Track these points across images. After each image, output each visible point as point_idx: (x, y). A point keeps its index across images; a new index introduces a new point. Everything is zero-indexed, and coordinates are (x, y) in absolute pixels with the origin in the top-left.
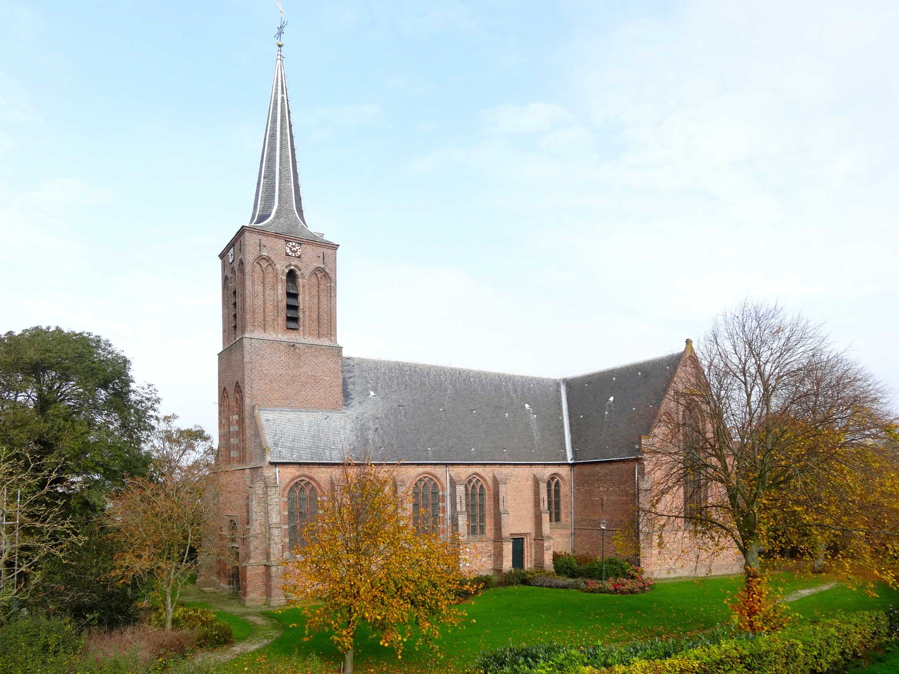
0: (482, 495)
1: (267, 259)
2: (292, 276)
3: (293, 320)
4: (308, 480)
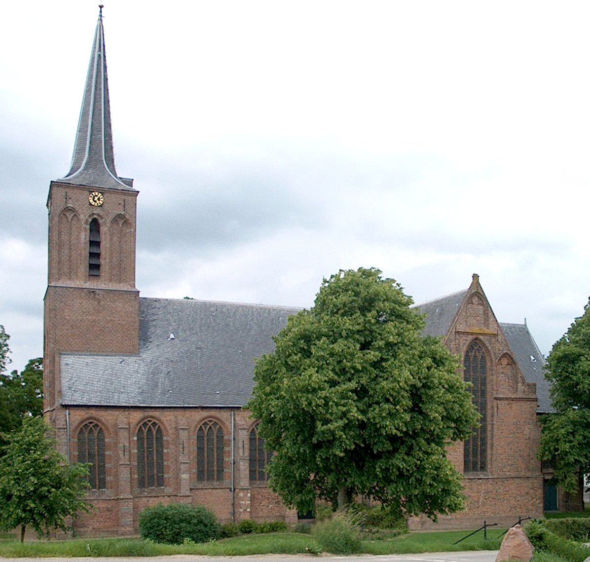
1: (72, 210)
2: (95, 226)
3: (94, 268)
4: (96, 422)
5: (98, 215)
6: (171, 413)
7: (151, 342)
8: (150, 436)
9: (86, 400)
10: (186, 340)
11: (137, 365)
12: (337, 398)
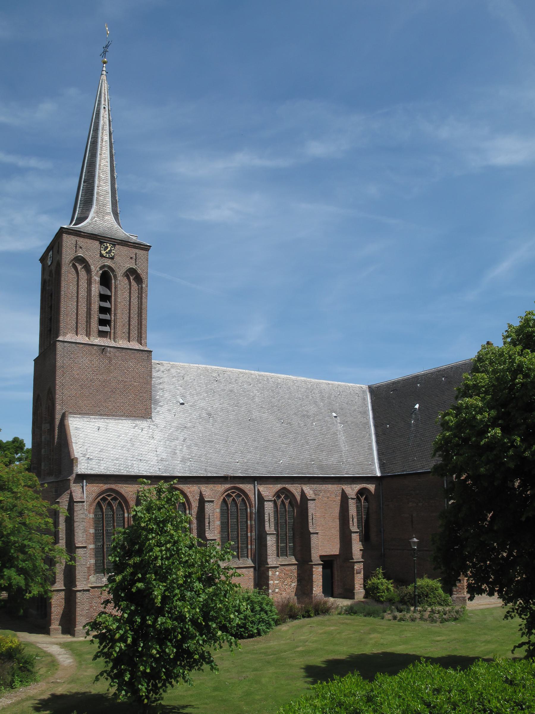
5: (110, 267)
7: (161, 406)
9: (104, 469)
11: (151, 431)
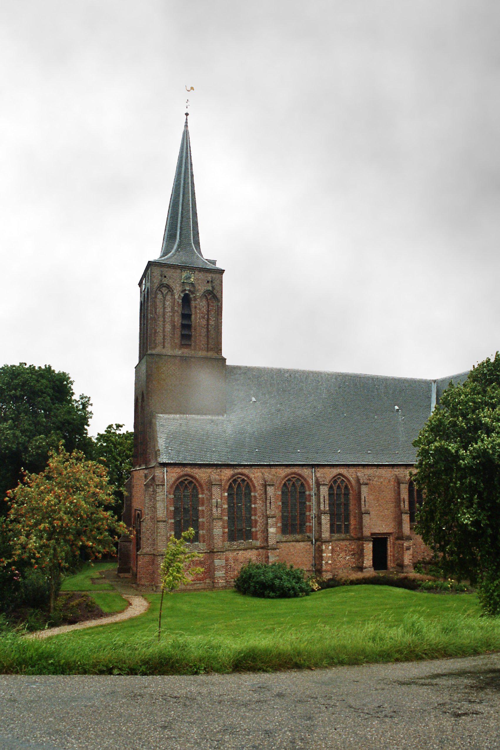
0: (347, 495)
1: (168, 287)
6: (258, 470)
8: (240, 490)
10: (267, 403)
12: (107, 477)
